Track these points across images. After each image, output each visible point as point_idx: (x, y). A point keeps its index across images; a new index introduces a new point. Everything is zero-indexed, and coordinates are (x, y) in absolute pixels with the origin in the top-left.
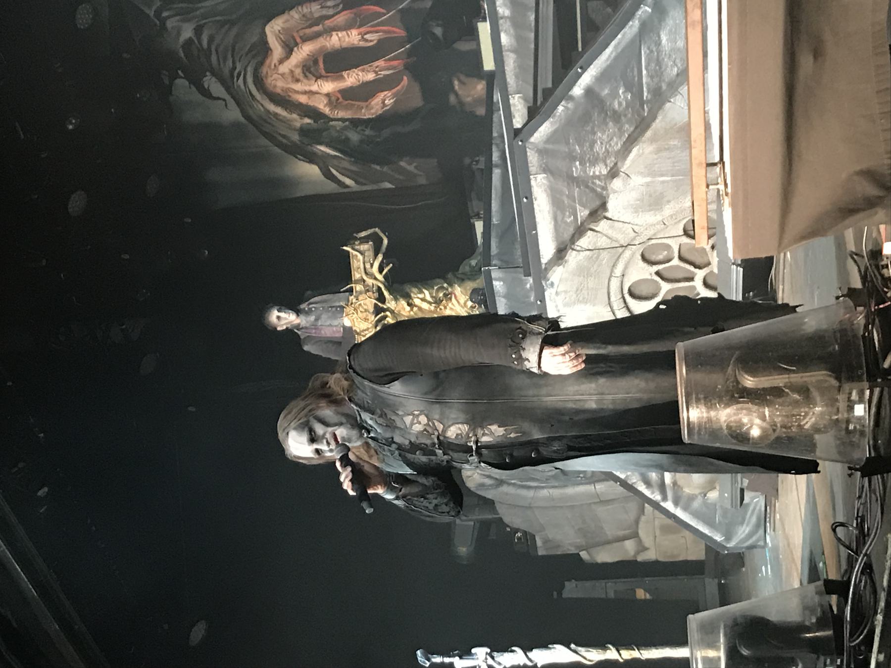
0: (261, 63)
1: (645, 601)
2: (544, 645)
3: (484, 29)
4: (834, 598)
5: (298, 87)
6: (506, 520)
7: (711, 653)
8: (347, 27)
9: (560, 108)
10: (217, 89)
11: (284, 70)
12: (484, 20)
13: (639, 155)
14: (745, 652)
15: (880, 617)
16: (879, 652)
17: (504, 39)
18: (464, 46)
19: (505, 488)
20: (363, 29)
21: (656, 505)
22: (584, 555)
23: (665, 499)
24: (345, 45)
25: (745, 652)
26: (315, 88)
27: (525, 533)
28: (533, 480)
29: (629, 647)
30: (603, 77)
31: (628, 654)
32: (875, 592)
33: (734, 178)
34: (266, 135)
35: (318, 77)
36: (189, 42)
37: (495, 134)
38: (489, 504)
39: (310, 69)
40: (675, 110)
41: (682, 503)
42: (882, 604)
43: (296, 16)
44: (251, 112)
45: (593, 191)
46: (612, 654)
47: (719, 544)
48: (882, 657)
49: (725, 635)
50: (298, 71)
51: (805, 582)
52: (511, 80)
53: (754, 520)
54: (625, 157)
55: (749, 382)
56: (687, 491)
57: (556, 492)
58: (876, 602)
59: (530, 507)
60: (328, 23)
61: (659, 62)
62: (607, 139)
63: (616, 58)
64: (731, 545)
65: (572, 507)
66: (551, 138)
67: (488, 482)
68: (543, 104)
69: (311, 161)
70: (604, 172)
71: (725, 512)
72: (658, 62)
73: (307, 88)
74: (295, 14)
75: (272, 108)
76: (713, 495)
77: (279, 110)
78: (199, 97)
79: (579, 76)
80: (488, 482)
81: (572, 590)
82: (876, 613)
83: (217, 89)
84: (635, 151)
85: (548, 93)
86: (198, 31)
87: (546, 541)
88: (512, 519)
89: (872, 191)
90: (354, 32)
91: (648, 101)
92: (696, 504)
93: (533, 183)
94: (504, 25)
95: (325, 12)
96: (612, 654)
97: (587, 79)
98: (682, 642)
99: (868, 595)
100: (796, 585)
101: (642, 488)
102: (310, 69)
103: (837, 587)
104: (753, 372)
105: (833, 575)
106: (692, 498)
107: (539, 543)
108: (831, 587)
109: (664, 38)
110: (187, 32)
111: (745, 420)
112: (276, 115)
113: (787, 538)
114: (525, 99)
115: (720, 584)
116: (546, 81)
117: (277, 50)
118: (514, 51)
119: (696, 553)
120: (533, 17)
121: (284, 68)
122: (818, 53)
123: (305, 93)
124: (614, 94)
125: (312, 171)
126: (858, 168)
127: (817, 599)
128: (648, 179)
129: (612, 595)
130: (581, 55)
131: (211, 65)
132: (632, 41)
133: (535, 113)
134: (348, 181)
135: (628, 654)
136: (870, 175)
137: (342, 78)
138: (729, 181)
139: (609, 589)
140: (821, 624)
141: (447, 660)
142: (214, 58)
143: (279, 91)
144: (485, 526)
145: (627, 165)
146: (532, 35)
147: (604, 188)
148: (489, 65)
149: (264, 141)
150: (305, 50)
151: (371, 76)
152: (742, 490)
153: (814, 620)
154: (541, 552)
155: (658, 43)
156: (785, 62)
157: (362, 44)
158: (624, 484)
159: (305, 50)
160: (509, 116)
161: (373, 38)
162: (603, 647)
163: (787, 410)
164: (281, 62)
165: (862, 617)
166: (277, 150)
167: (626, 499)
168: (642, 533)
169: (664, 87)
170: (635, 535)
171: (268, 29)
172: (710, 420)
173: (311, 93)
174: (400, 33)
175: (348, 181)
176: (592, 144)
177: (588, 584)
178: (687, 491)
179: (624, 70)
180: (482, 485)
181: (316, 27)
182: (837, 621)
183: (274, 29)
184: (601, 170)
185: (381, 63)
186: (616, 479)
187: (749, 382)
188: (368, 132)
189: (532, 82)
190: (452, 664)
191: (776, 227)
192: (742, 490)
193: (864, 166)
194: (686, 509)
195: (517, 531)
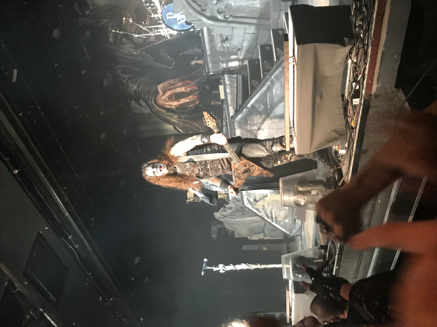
0: (157, 96)
1: (266, 251)
2: (239, 264)
3: (221, 87)
4: (323, 251)
5: (167, 103)
6: (227, 227)
7: (288, 266)
8: (181, 87)
9: (244, 110)
10: (143, 104)
11: (163, 99)
12: (221, 84)
13: (267, 124)
14: (298, 266)
15: (337, 256)
16: (337, 266)
17: (228, 91)
18: (215, 92)
19: (226, 218)
20: (186, 87)
21: (270, 223)
22: (249, 237)
23: (273, 221)
24: (180, 91)
25: (298, 266)
26: (172, 104)
27: (232, 231)
28: (234, 216)
29: (264, 264)
30: (256, 102)
31: (263, 266)
32: (335, 249)
33: (297, 132)
34: (158, 117)
35: (173, 101)
36: (135, 90)
37: (224, 117)
38: (222, 223)
39: (170, 98)
40: (278, 111)
41: (278, 222)
42: (337, 252)
43: (167, 83)
44: (153, 110)
45: (253, 134)
46: (259, 266)
47: (288, 235)
48: (337, 267)
49: (292, 261)
50: (167, 99)
51: (314, 246)
52: (229, 102)
53: (298, 228)
54: (262, 125)
55: (301, 189)
56: (279, 219)
57: (241, 219)
58: (336, 251)
59: (233, 224)
60: (176, 85)
61: (272, 98)
62: (257, 119)
63: (260, 97)
64: (291, 235)
65: (245, 224)
66: (241, 119)
67: (221, 216)
68: (239, 109)
69: (170, 124)
70: (257, 128)
71: (290, 225)
72: (272, 98)
73: (169, 104)
74: (166, 83)
75: (159, 109)
76: (287, 221)
77: (161, 110)
78: (139, 106)
79: (250, 101)
80: (221, 216)
81: (245, 247)
82: (335, 255)
83: (143, 104)
84: (265, 123)
85: (241, 106)
86: (138, 87)
87: (238, 234)
88: (228, 227)
89: (336, 136)
90: (183, 88)
91: (269, 109)
92: (282, 223)
93: (236, 131)
94: (228, 87)
95: (175, 82)
96: (259, 266)
97: (252, 102)
98: (280, 263)
99: (333, 250)
100: (311, 247)
101: (266, 218)
102: (170, 98)
103: (324, 247)
104: (302, 186)
105: (322, 244)
106: (280, 221)
107: (236, 234)
108: (322, 247)
109: (274, 91)
110: (135, 87)
111: (299, 200)
112: (160, 111)
113: (308, 233)
114: (234, 108)
115: (287, 246)
116: (240, 103)
117: (161, 93)
118: (231, 94)
119: (281, 237)
120: (236, 84)
121: (163, 98)
122: (321, 97)
123: (169, 105)
124: (260, 107)
125: (171, 127)
126: (332, 129)
127: (318, 251)
128: (269, 131)
129: (256, 249)
130: (250, 95)
131: (141, 96)
132: (265, 92)
133: (237, 112)
134: (181, 131)
135: (263, 266)
136: (335, 131)
137: (179, 101)
138: (296, 132)
139: (255, 247)
140: (319, 258)
141: (211, 268)
142: (143, 95)
143: (161, 104)
144: (220, 229)
145: (262, 127)
146: (236, 90)
147: (256, 133)
148: (222, 97)
149: (157, 118)
150: (169, 93)
151: (188, 101)
152: (295, 219)
153: (317, 257)
154: (236, 237)
155: (272, 92)
156: (312, 100)
157: (185, 91)
158: (261, 217)
159: (169, 93)
160: (229, 113)
161: (188, 90)
162: (256, 264)
163: (311, 197)
164: (162, 96)
165: (331, 256)
166: (161, 121)
167: (261, 221)
168: (265, 231)
169: (274, 104)
170: (264, 232)
171: (158, 87)
172: (290, 200)
173: (170, 105)
174: (197, 88)
175: (181, 131)
176: (253, 120)
177: (249, 246)
178: (279, 219)
179: (262, 100)
180: (220, 217)
181: (172, 86)
182: (324, 257)
183: (160, 87)
184: (255, 128)
185: (191, 97)
186: (259, 216)
187: (301, 189)
188: (187, 116)
189: (236, 103)
190: (213, 269)
191: (309, 146)
192: (295, 219)
193: (334, 129)
194: (279, 224)
195: (230, 230)
